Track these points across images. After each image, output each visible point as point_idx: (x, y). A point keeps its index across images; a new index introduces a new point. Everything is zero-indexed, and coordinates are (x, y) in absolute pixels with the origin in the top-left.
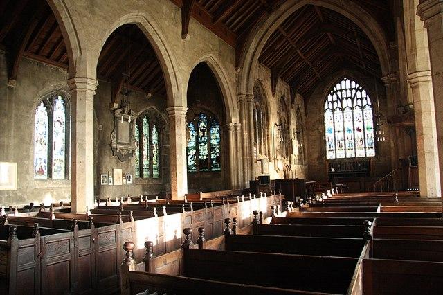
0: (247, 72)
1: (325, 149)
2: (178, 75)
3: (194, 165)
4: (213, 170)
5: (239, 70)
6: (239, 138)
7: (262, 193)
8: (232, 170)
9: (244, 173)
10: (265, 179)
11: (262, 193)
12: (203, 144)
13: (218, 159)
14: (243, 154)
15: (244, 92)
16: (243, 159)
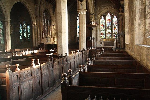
0: (39, 6)
1: (77, 33)
2: (5, 7)
3: (22, 39)
4: (28, 41)
5: (36, 5)
6: (36, 30)
7: (50, 49)
8: (34, 41)
9: (38, 42)
10: (43, 44)
11: (50, 49)
12: (25, 32)
13: (30, 37)
14: (38, 36)
15: (38, 13)
16: (38, 37)
